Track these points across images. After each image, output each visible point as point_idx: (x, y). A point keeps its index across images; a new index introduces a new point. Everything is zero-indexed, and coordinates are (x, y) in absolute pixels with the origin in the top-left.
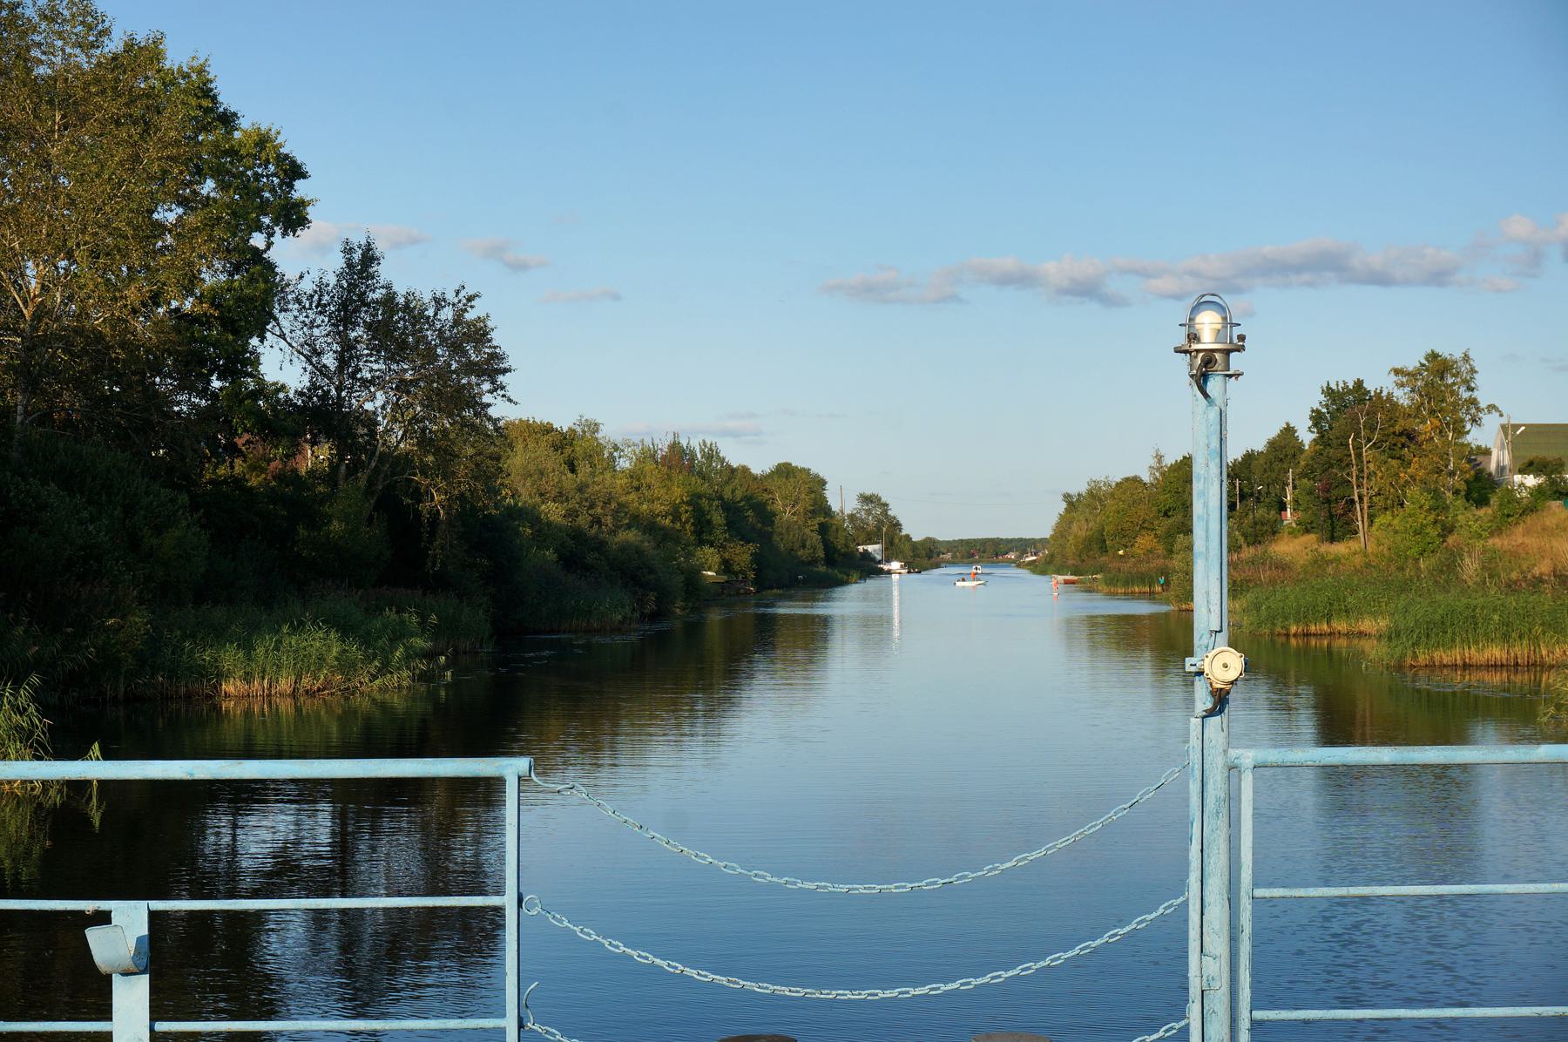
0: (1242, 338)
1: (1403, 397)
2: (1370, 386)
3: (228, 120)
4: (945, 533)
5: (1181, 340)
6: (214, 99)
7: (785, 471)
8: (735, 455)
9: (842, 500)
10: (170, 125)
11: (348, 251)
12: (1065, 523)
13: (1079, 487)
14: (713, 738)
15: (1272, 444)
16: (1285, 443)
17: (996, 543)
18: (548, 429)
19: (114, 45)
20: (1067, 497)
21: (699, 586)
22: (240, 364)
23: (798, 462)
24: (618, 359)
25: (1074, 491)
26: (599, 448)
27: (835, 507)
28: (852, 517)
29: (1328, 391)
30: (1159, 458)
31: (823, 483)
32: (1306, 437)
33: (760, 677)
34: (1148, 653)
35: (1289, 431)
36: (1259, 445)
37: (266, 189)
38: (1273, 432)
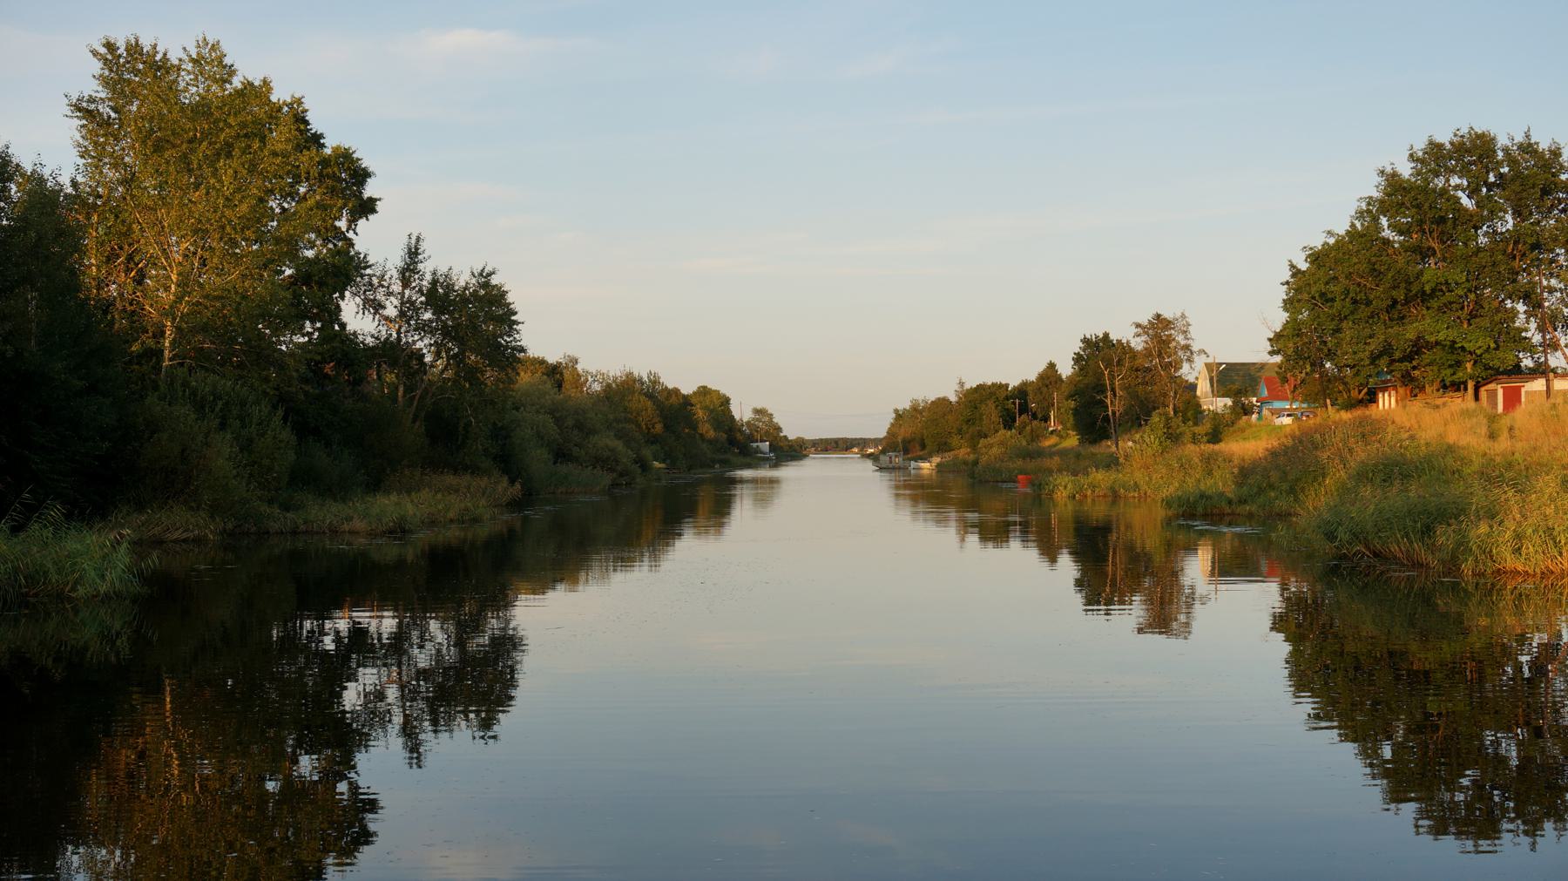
1: (1138, 344)
2: (1114, 337)
3: (317, 139)
4: (810, 435)
6: (307, 123)
7: (704, 391)
8: (669, 382)
9: (742, 411)
10: (279, 138)
11: (95, 53)
13: (905, 405)
14: (719, 533)
15: (1042, 377)
16: (1050, 375)
17: (845, 440)
18: (542, 362)
19: (237, 82)
20: (896, 411)
21: (668, 463)
22: (331, 314)
23: (712, 386)
25: (900, 407)
27: (737, 417)
28: (748, 423)
29: (1085, 341)
30: (962, 384)
31: (727, 401)
32: (1066, 369)
33: (596, 564)
34: (953, 524)
35: (1052, 366)
36: (1032, 376)
37: (346, 184)
38: (1042, 367)
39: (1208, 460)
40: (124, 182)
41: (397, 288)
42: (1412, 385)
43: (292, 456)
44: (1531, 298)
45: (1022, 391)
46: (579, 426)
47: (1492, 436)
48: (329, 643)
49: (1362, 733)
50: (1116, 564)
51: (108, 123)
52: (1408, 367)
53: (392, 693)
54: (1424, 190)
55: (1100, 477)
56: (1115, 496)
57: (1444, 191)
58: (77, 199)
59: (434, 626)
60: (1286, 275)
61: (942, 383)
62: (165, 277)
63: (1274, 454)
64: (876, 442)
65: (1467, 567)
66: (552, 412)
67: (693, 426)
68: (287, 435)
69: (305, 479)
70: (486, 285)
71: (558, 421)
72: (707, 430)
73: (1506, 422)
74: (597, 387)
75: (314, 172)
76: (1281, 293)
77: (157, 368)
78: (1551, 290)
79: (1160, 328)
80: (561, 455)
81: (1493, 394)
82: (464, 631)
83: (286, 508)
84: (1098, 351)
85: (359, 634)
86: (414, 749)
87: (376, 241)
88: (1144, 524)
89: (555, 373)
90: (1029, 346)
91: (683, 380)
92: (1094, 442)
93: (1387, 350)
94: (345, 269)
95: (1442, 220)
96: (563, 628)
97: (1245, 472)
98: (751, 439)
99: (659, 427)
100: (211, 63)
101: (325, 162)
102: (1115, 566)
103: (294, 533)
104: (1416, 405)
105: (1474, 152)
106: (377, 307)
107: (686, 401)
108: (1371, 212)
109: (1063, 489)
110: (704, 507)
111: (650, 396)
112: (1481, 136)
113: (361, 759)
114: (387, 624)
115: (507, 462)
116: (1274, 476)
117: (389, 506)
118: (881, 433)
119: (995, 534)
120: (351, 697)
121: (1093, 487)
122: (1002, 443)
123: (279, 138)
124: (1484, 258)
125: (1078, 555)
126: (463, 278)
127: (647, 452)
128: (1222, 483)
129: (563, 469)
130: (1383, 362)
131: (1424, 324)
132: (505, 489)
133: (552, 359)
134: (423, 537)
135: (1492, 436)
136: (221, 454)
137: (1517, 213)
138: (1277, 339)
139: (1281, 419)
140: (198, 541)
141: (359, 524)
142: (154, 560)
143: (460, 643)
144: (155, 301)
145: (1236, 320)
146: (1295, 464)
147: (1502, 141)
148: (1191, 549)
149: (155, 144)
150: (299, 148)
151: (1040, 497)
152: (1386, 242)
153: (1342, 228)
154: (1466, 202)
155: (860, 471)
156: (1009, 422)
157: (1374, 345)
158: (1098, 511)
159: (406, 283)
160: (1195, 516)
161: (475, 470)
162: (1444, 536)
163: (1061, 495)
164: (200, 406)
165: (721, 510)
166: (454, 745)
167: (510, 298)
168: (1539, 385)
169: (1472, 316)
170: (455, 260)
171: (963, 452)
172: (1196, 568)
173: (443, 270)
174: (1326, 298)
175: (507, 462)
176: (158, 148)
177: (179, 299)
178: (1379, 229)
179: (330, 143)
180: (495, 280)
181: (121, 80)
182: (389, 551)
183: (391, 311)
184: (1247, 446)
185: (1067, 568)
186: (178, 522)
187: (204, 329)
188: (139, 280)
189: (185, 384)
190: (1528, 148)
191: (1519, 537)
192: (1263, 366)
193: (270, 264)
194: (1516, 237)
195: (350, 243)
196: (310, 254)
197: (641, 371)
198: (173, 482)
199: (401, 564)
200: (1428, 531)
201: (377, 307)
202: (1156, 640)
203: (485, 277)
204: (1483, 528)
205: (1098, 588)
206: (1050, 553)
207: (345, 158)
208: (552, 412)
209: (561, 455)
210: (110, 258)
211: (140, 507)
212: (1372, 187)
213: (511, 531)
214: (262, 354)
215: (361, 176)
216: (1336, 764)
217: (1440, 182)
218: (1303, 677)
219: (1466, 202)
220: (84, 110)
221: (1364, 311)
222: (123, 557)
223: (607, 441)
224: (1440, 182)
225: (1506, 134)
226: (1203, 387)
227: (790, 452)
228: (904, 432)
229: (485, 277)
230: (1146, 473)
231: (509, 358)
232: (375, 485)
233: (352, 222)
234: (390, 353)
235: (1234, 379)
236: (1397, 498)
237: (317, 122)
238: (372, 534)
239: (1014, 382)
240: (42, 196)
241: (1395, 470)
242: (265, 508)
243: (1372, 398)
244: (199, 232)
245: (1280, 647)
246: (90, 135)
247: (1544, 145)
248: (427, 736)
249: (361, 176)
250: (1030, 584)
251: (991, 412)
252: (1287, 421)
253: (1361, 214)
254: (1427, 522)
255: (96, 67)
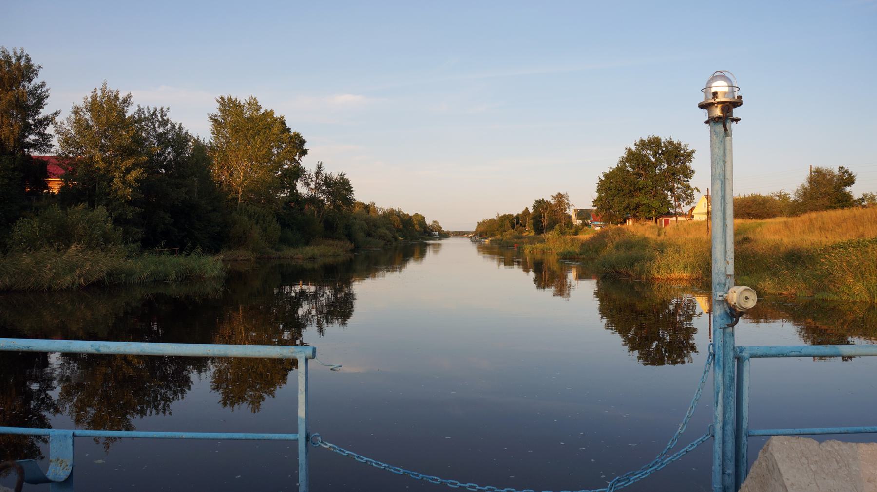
0: (740, 97)
1: (553, 202)
3: (289, 129)
5: (702, 99)
7: (417, 215)
9: (429, 222)
10: (276, 129)
12: (477, 230)
13: (481, 221)
14: (422, 260)
15: (524, 212)
19: (262, 111)
21: (404, 238)
22: (293, 187)
24: (378, 189)
26: (274, 385)
32: (531, 210)
35: (527, 209)
36: (521, 212)
37: (298, 145)
39: (573, 240)
40: (226, 143)
41: (314, 179)
42: (636, 218)
43: (280, 233)
44: (671, 190)
45: (518, 217)
46: (375, 225)
47: (659, 235)
48: (293, 294)
49: (623, 332)
50: (546, 275)
51: (220, 123)
52: (636, 212)
53: (314, 312)
54: (640, 155)
55: (538, 245)
56: (543, 252)
57: (645, 155)
58: (213, 149)
59: (327, 290)
60: (598, 181)
61: (493, 214)
62: (239, 174)
63: (592, 239)
64: (472, 233)
65: (643, 277)
66: (365, 221)
67: (413, 226)
68: (278, 226)
69: (284, 241)
70: (343, 178)
71: (368, 224)
72: (417, 228)
73: (663, 230)
74: (380, 213)
75: (288, 140)
76: (596, 187)
77: (237, 204)
78: (678, 188)
79: (560, 197)
80: (369, 235)
81: (661, 221)
82: (336, 291)
83: (277, 250)
84: (541, 204)
85: (302, 292)
86: (321, 330)
87: (308, 163)
88: (552, 261)
89: (367, 208)
90: (519, 203)
91: (409, 210)
92: (539, 234)
93: (628, 206)
94: (297, 172)
95: (645, 165)
96: (371, 292)
97: (583, 244)
98: (432, 231)
99: (401, 226)
100: (254, 105)
101: (291, 137)
102: (547, 276)
103: (279, 258)
104: (637, 225)
105: (654, 143)
106: (308, 185)
107: (411, 218)
108: (623, 161)
109: (527, 248)
110: (416, 254)
111: (399, 216)
112: (656, 138)
113: (304, 332)
114: (311, 289)
115: (350, 237)
116: (591, 246)
117: (310, 250)
118: (474, 230)
119: (509, 263)
120: (301, 312)
121: (537, 248)
122: (510, 234)
123: (276, 129)
124: (658, 177)
125: (534, 271)
126: (335, 176)
127: (397, 235)
128: (576, 249)
129: (369, 239)
130: (628, 210)
131: (639, 198)
132: (349, 245)
133: (366, 203)
134: (320, 261)
135: (659, 235)
136: (256, 232)
137: (668, 163)
138: (595, 202)
139: (598, 227)
140: (247, 260)
141: (300, 256)
142: (229, 267)
143: (335, 295)
144: (236, 182)
145: (583, 196)
146: (600, 240)
147: (663, 140)
148: (569, 269)
149: (236, 130)
150: (283, 133)
151: (520, 253)
152: (628, 171)
153: (614, 166)
154: (652, 159)
155: (466, 241)
156: (513, 227)
157: (625, 204)
158: (539, 257)
159: (317, 177)
160: (568, 258)
161: (339, 239)
162: (637, 267)
163: (526, 251)
164: (250, 216)
165: (422, 254)
166: (334, 329)
167: (351, 183)
168: (674, 219)
169: (654, 196)
170: (333, 170)
171: (499, 237)
172: (572, 276)
173: (329, 173)
174: (610, 189)
175: (350, 237)
176: (236, 132)
177: (243, 181)
178: (626, 167)
179: (293, 131)
180: (345, 177)
181: (226, 109)
182: (309, 265)
183: (313, 186)
184: (584, 237)
185: (532, 275)
186: (242, 254)
187: (251, 191)
188: (231, 175)
189: (245, 209)
190: (671, 142)
191: (659, 267)
192: (592, 210)
193: (273, 170)
194: (667, 170)
195: (299, 164)
196: (286, 167)
197: (396, 208)
198: (241, 241)
199: (314, 269)
200: (632, 264)
201: (308, 185)
202: (559, 299)
203: (342, 176)
204: (648, 264)
205: (541, 282)
206: (526, 270)
207: (297, 136)
208: (365, 221)
209: (369, 235)
210: (222, 167)
211: (230, 249)
212: (623, 154)
213: (351, 259)
214: (270, 200)
215: (303, 142)
216: (616, 339)
217: (644, 153)
218: (604, 312)
219: (652, 159)
220: (214, 119)
221: (621, 193)
222: (219, 265)
223: (383, 231)
224: (644, 153)
225: (664, 138)
226: (574, 217)
227: (445, 235)
228: (481, 229)
229: (342, 176)
230: (553, 243)
231: (349, 202)
232: (307, 243)
233: (300, 157)
234: (312, 200)
235: (583, 214)
236: (623, 253)
237: (288, 125)
238: (304, 259)
239: (515, 214)
240: (199, 147)
241: (629, 245)
242: (270, 250)
243: (625, 222)
244: (250, 159)
245: (596, 303)
246: (215, 127)
247: (675, 142)
248: (325, 325)
249: (303, 142)
250: (520, 279)
251: (508, 224)
252: (599, 228)
253: (620, 162)
254: (632, 262)
255: (218, 105)
